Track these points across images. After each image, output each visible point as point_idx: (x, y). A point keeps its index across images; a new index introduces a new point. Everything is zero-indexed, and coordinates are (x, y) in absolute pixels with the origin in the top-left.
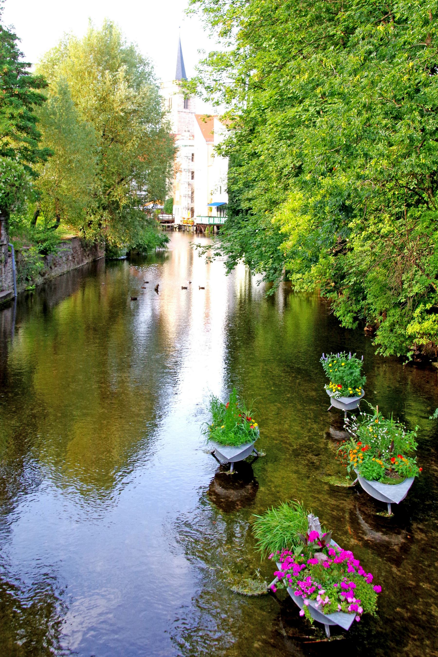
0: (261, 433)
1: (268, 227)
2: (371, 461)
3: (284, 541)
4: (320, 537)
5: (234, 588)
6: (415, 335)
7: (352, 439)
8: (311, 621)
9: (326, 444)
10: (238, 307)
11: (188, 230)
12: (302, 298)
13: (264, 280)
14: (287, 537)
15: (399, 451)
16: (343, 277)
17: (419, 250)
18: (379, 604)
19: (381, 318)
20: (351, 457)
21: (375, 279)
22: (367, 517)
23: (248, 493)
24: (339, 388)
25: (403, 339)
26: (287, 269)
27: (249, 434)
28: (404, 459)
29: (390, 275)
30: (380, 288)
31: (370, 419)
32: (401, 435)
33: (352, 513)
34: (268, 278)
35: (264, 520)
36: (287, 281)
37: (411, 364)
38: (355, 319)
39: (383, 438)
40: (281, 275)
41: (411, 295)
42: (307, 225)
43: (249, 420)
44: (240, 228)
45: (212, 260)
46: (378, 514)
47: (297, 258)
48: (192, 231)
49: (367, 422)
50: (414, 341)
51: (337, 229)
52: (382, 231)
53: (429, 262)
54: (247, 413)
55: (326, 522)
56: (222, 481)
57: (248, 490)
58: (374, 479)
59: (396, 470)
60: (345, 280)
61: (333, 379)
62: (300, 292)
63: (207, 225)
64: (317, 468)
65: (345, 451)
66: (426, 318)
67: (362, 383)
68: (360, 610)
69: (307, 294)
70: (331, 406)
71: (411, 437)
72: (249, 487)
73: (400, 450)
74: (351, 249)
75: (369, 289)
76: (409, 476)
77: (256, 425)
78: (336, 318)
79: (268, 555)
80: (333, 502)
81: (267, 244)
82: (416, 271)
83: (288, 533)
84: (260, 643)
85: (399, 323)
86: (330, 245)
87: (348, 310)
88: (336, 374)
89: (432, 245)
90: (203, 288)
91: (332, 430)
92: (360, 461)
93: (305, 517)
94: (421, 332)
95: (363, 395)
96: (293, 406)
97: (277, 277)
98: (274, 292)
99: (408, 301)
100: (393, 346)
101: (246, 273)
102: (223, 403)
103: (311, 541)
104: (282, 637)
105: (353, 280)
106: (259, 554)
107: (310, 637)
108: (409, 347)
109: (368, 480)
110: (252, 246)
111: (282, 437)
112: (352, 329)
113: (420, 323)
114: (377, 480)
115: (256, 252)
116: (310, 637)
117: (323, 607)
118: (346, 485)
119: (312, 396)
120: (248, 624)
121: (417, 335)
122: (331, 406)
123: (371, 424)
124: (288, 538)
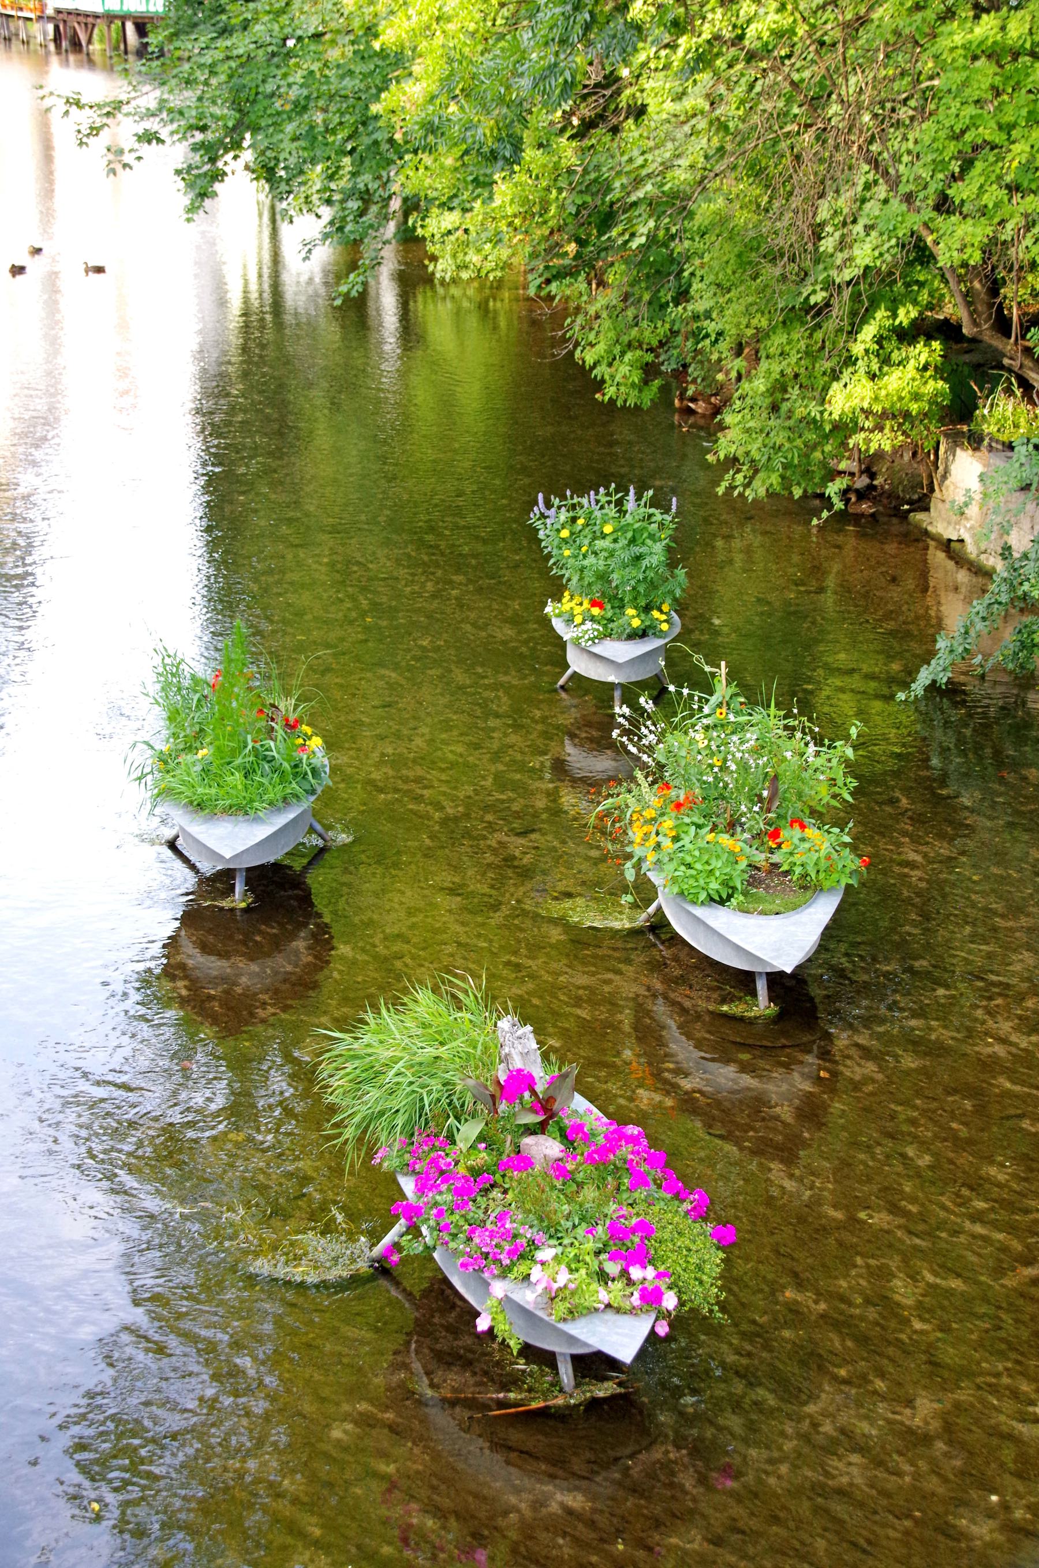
0: (334, 769)
1: (333, 25)
2: (701, 843)
3: (422, 1108)
4: (540, 1088)
5: (262, 1266)
6: (854, 421)
7: (639, 775)
8: (514, 1345)
9: (553, 796)
10: (235, 340)
11: (23, 35)
12: (466, 304)
13: (326, 236)
14: (430, 1093)
15: (794, 808)
16: (607, 220)
17: (882, 104)
18: (728, 1278)
19: (739, 364)
20: (636, 834)
21: (722, 220)
22: (688, 1019)
23: (296, 966)
24: (596, 611)
25: (811, 436)
26: (408, 192)
27: (295, 775)
28: (811, 832)
29: (776, 204)
30: (739, 256)
31: (701, 709)
32: (802, 755)
33: (641, 1011)
34: (340, 229)
35: (356, 1046)
36: (410, 240)
37: (842, 517)
38: (650, 371)
39: (744, 766)
40: (386, 218)
41: (847, 274)
42: (478, 16)
43: (291, 726)
44: (225, 31)
45: (128, 158)
46: (725, 1008)
47: (442, 149)
48: (40, 39)
49: (692, 716)
50: (851, 442)
51: (587, 27)
52: (751, 32)
53: (918, 148)
54: (286, 705)
55: (552, 1042)
56: (209, 931)
57: (297, 953)
58: (712, 900)
59: (785, 868)
60: (614, 233)
61: (575, 579)
62: (454, 281)
63: (96, 16)
64: (525, 874)
65: (616, 814)
66: (895, 356)
67: (671, 592)
68: (670, 1301)
69: (481, 288)
70: (569, 672)
71: (835, 761)
72: (300, 944)
73: (799, 805)
74: (639, 112)
75: (697, 262)
76: (827, 884)
77: (316, 743)
78: (583, 371)
79: (371, 1154)
80: (583, 980)
81: (331, 97)
82: (867, 187)
83: (433, 1082)
84: (349, 1426)
85: (802, 379)
86: (564, 95)
87: (625, 339)
88: (586, 563)
89: (931, 78)
90: (100, 270)
91: (574, 755)
92: (667, 843)
93: (489, 1027)
94: (877, 408)
95: (677, 630)
96: (441, 677)
97: (371, 226)
98: (365, 284)
99: (835, 301)
100: (778, 461)
101: (260, 215)
102: (200, 675)
103: (511, 1101)
104: (421, 1403)
105: (644, 230)
106: (341, 1153)
107: (512, 1395)
108: (832, 463)
109: (695, 903)
110: (278, 104)
111: (406, 780)
112: (637, 408)
113: (873, 377)
114: (722, 902)
115: (290, 128)
116: (512, 1395)
117: (552, 1299)
118: (621, 923)
119: (504, 643)
120: (308, 1371)
121: (861, 418)
122: (569, 672)
123: (705, 721)
124: (435, 1095)
